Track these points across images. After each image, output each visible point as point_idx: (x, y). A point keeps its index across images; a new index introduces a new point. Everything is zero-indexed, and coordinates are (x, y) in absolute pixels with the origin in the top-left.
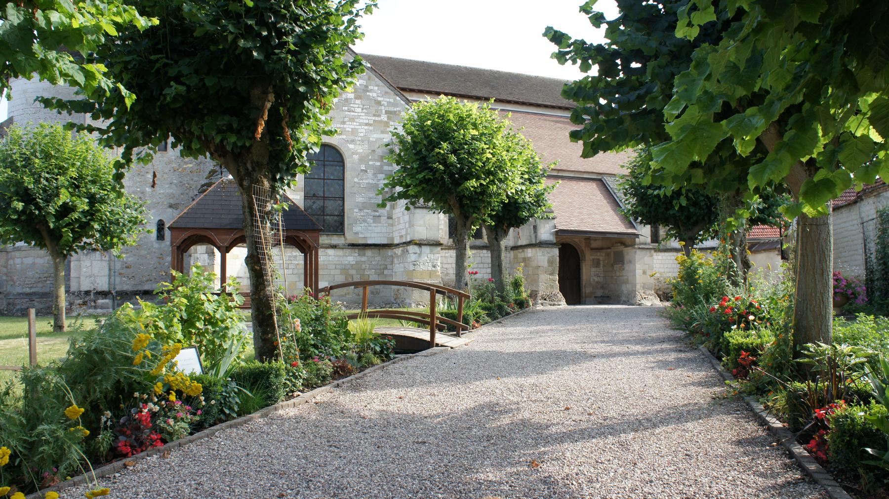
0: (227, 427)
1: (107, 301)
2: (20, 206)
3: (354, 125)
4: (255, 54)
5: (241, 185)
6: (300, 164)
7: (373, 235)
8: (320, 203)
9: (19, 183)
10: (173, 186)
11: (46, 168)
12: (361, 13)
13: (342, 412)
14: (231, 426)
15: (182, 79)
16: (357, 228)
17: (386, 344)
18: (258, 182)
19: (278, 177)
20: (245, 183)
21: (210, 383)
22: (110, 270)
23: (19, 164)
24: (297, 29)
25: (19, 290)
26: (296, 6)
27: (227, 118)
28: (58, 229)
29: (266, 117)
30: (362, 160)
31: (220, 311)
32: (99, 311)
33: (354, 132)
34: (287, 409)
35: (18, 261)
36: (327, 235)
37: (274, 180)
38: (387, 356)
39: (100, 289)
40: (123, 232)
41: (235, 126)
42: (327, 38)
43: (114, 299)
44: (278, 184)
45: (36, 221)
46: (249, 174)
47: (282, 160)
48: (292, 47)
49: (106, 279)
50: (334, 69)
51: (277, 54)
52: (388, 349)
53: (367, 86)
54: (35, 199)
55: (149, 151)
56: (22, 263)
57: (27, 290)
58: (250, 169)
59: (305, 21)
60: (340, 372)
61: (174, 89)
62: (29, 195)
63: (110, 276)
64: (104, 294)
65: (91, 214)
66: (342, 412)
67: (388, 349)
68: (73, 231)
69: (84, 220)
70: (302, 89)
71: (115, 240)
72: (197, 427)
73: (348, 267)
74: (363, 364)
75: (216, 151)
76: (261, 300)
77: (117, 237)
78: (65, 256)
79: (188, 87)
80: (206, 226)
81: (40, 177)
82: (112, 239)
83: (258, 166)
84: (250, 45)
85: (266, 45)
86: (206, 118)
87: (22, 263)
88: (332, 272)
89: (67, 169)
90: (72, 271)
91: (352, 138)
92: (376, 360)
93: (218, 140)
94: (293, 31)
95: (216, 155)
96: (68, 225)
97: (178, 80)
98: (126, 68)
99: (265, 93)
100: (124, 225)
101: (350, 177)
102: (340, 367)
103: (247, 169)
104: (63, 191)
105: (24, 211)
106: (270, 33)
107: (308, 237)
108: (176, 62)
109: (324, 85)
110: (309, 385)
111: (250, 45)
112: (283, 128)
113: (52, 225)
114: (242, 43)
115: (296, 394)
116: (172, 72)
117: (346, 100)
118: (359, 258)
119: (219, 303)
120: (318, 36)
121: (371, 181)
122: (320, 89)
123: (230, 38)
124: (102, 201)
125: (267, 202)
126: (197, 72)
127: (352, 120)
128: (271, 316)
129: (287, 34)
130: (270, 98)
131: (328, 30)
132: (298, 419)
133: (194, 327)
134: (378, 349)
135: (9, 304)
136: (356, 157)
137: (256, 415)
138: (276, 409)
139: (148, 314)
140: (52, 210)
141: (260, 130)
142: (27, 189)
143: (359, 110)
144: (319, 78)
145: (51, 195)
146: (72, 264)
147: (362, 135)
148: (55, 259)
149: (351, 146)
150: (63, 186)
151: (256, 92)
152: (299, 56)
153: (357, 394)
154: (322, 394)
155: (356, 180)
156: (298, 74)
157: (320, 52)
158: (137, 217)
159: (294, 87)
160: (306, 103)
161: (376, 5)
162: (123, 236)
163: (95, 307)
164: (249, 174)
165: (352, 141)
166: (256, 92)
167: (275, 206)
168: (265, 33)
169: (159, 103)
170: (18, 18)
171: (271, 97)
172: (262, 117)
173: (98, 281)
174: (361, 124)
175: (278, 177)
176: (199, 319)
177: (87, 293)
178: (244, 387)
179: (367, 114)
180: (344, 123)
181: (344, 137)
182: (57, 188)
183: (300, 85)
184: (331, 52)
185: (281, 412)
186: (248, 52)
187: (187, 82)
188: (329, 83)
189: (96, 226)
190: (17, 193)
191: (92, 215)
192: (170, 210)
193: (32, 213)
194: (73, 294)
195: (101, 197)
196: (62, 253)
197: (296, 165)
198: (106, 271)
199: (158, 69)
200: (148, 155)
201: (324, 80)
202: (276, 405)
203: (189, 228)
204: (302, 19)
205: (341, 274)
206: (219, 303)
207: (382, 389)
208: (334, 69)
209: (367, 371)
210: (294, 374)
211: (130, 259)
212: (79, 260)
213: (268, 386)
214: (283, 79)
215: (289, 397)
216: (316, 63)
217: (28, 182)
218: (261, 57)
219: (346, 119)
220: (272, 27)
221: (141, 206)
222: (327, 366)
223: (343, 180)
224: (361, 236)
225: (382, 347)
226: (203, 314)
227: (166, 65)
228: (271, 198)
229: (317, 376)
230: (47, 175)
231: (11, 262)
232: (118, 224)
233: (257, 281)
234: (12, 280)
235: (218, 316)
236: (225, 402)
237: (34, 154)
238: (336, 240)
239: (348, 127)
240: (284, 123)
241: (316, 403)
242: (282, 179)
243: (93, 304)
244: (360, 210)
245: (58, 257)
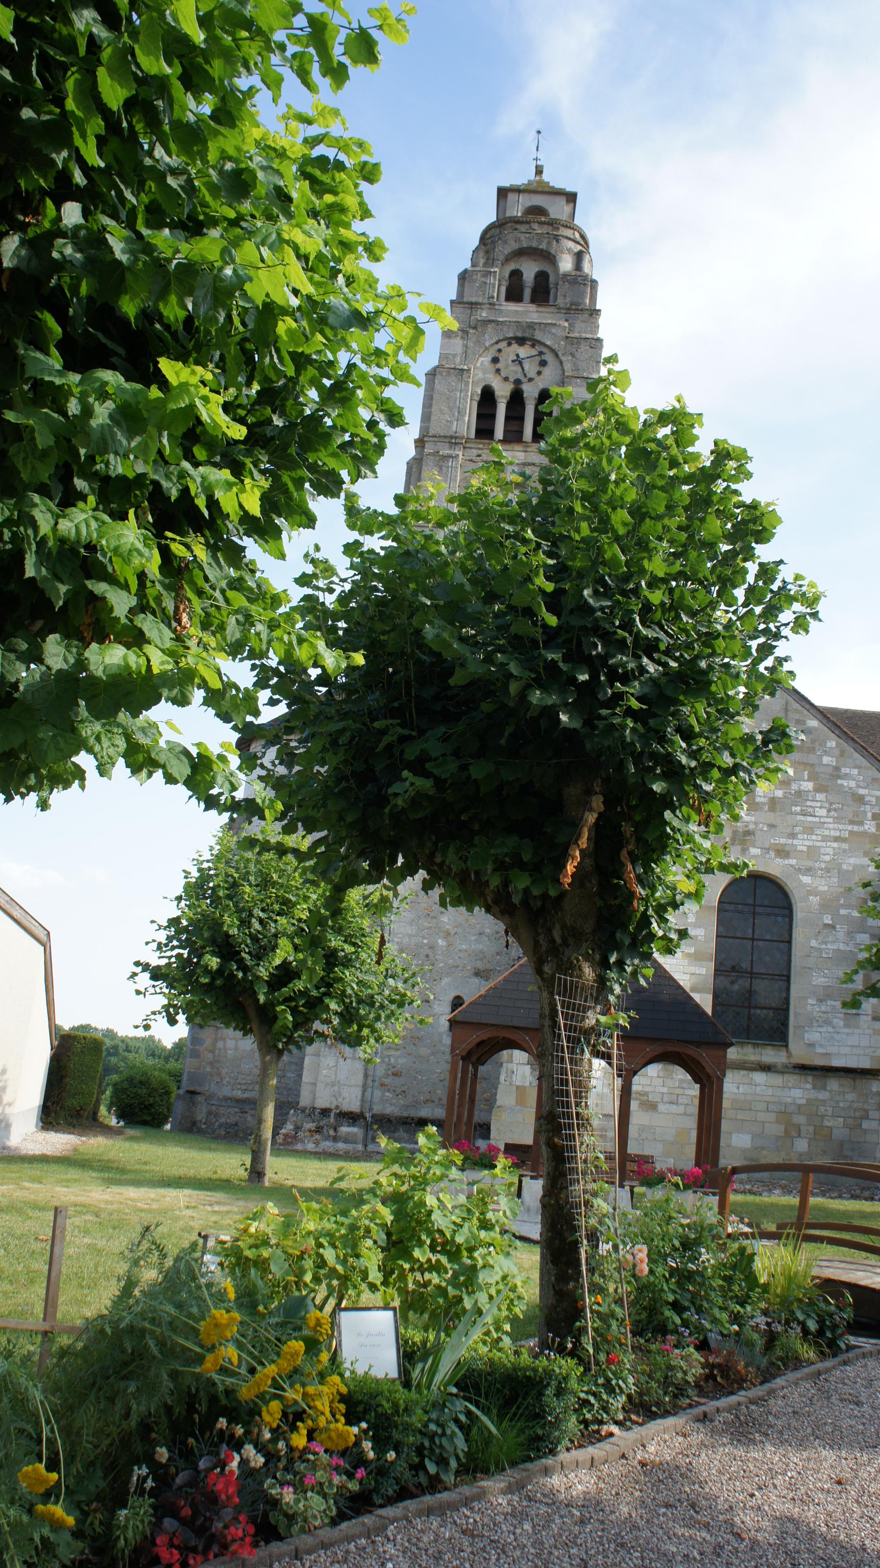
0: (419, 1514)
1: (354, 1130)
2: (214, 962)
3: (813, 840)
4: (564, 718)
5: (539, 971)
6: (660, 933)
7: (843, 1050)
8: (740, 985)
9: (216, 925)
10: (485, 939)
11: (262, 901)
12: (785, 631)
13: (693, 1506)
14: (429, 1512)
15: (428, 766)
16: (813, 1036)
17: (831, 1315)
18: (570, 968)
19: (612, 960)
20: (547, 969)
21: (395, 1405)
22: (366, 1076)
23: (221, 894)
24: (651, 668)
25: (226, 1091)
26: (643, 624)
27: (512, 841)
28: (271, 1005)
29: (583, 842)
30: (827, 905)
31: (465, 1229)
32: (341, 1145)
33: (813, 852)
34: (574, 1475)
35: (230, 1044)
36: (755, 1045)
37: (604, 964)
38: (832, 1344)
39: (346, 1107)
40: (378, 1018)
41: (526, 857)
42: (710, 683)
43: (367, 1127)
44: (612, 975)
45: (238, 989)
46: (555, 951)
47: (625, 927)
48: (635, 704)
49: (358, 1092)
50: (726, 747)
51: (605, 718)
52: (835, 1327)
53: (837, 769)
54: (239, 953)
55: (385, 893)
56: (236, 1048)
57: (239, 1094)
58: (558, 940)
59: (668, 652)
60: (720, 1379)
61: (409, 785)
62: (232, 946)
63: (364, 1087)
64: (352, 1118)
65: (328, 984)
66: (693, 1506)
67: (835, 1327)
68: (294, 1011)
69: (314, 993)
70: (657, 787)
71: (366, 1032)
72: (355, 1505)
73: (791, 1109)
74: (775, 1361)
75: (496, 902)
76: (561, 1208)
77: (369, 1026)
78: (280, 1053)
79: (438, 781)
80: (516, 1023)
81: (251, 915)
82: (360, 1030)
83: (574, 936)
84: (553, 699)
85: (587, 699)
86: (476, 840)
87: (236, 1048)
88: (761, 1116)
89: (294, 905)
90: (305, 1073)
91: (809, 863)
92: (808, 1352)
93: (495, 882)
94: (642, 670)
95: (496, 909)
96: (288, 1000)
97: (419, 767)
98: (334, 743)
99: (589, 792)
100: (382, 1007)
101: (804, 939)
102: (719, 1366)
103: (553, 941)
104: (283, 942)
105: (220, 971)
106: (594, 677)
107: (704, 1056)
108: (422, 732)
109: (706, 780)
110: (644, 1409)
111: (553, 699)
112: (623, 865)
113: (262, 999)
114: (536, 696)
115: (605, 1429)
116: (411, 752)
117: (799, 793)
118: (813, 1094)
119: (469, 1211)
120: (693, 680)
121: (842, 947)
122: (698, 788)
123: (514, 688)
124: (347, 963)
125: (585, 1009)
126: (456, 754)
127: (809, 830)
128: (576, 1244)
129: (626, 679)
130: (594, 804)
131: (710, 668)
132: (592, 1506)
133: (409, 1257)
134: (812, 1325)
135: (210, 1113)
136: (814, 900)
137: (494, 1485)
138: (547, 1472)
139: (312, 1226)
140: (263, 972)
141: (570, 868)
142: (227, 935)
143: (823, 812)
144: (693, 764)
145: (264, 948)
146: (307, 1061)
147: (827, 858)
148: (263, 1056)
149: (806, 879)
150: (284, 934)
151: (573, 791)
152: (652, 722)
153: (740, 1452)
154: (662, 1440)
155: (814, 943)
156: (653, 755)
157: (695, 712)
158: (405, 995)
159: (644, 783)
160: (668, 815)
161: (815, 615)
162: (379, 1025)
163: (335, 1139)
164: (555, 951)
165: (809, 871)
166: (573, 791)
167: (603, 1019)
168: (583, 677)
169: (387, 810)
170: (66, 660)
171: (598, 802)
172: (576, 843)
173: (345, 1094)
174: (825, 839)
175: (612, 960)
176: (421, 1244)
177: (325, 1112)
178: (486, 1411)
179: (837, 820)
180: (793, 836)
181: (793, 862)
182: (276, 936)
183: (657, 778)
184: (726, 714)
185: (556, 1481)
186: (550, 713)
187: (436, 772)
188: (716, 774)
189: (333, 1006)
190: (213, 941)
191: (329, 985)
192: (476, 980)
193: (232, 976)
194: (303, 1110)
195: (346, 956)
196: (276, 1046)
197: (652, 936)
198: (359, 1078)
199: (389, 746)
200: (384, 899)
201: (706, 767)
202: (549, 1461)
203: (487, 1025)
204: (662, 647)
205: (778, 1122)
206: (469, 1211)
207: (802, 1444)
208: (726, 747)
209: (780, 1381)
210: (608, 1380)
211: (400, 1061)
212: (318, 1055)
213: (538, 1415)
214: (621, 766)
215: (591, 1434)
216: (688, 735)
217: (230, 924)
218: (577, 725)
219: (798, 829)
220: (594, 665)
221: (414, 975)
222: (689, 1363)
223: (790, 942)
224: (819, 1050)
225: (821, 1322)
226: (429, 1233)
227: (403, 739)
228: (597, 1001)
229: (666, 1382)
230: (261, 914)
231: (220, 1044)
232: (372, 1004)
233: (556, 1168)
234: (219, 1074)
235: (460, 1239)
236: (428, 1448)
237: (245, 877)
238: (769, 1055)
239: (802, 843)
240: (624, 853)
241: (643, 1464)
242: (620, 964)
243: (332, 1132)
244: (820, 1001)
245: (268, 1053)
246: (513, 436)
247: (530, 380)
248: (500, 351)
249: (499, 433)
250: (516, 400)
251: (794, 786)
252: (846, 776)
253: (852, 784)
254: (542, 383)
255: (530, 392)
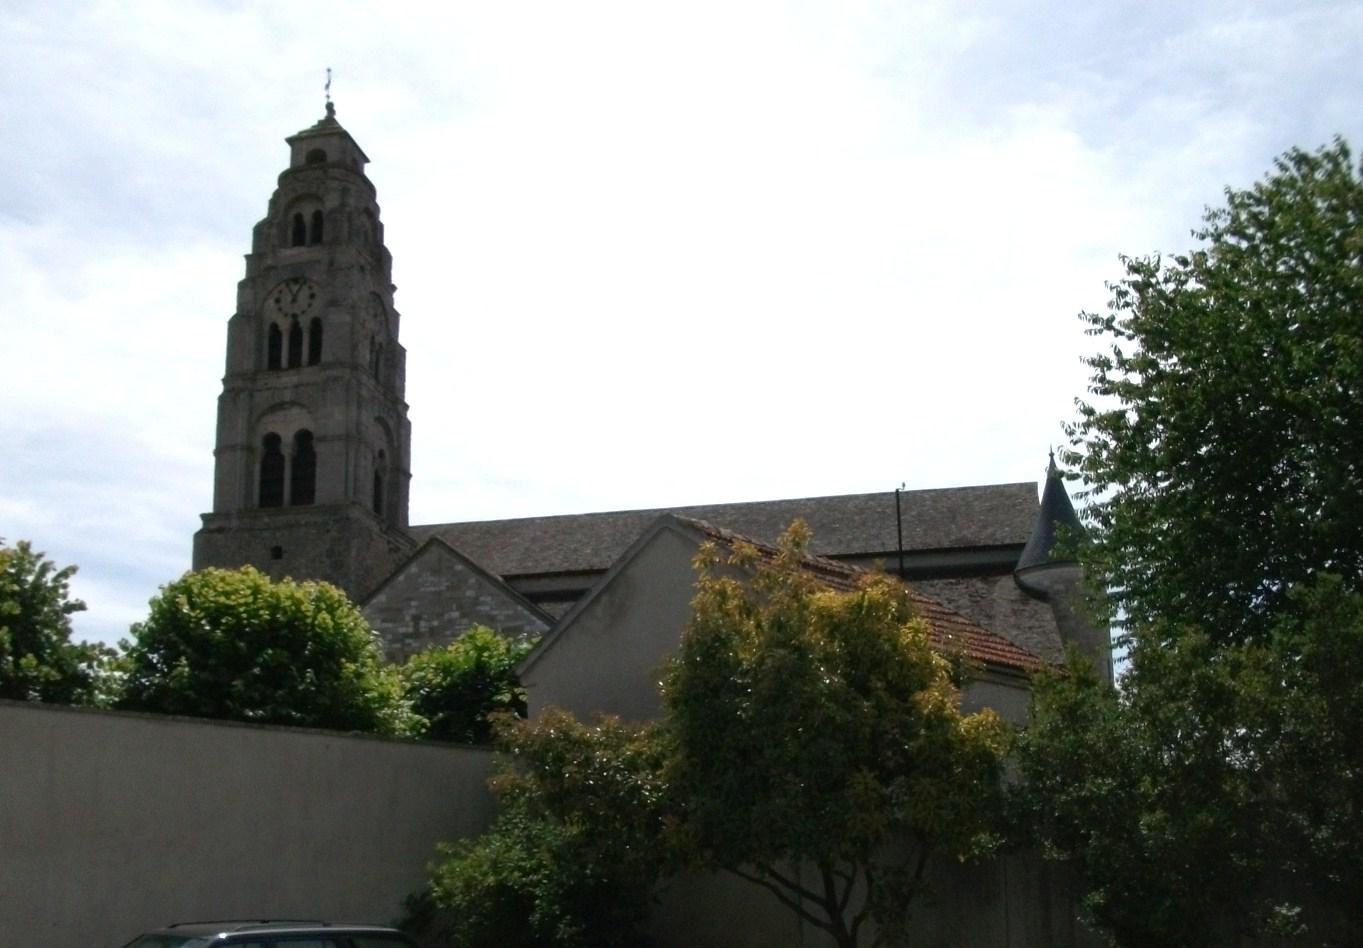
53: (477, 598)
246: (295, 363)
247: (303, 312)
248: (281, 292)
249: (284, 362)
250: (296, 332)
251: (446, 617)
252: (484, 603)
253: (487, 608)
254: (315, 312)
255: (305, 323)
